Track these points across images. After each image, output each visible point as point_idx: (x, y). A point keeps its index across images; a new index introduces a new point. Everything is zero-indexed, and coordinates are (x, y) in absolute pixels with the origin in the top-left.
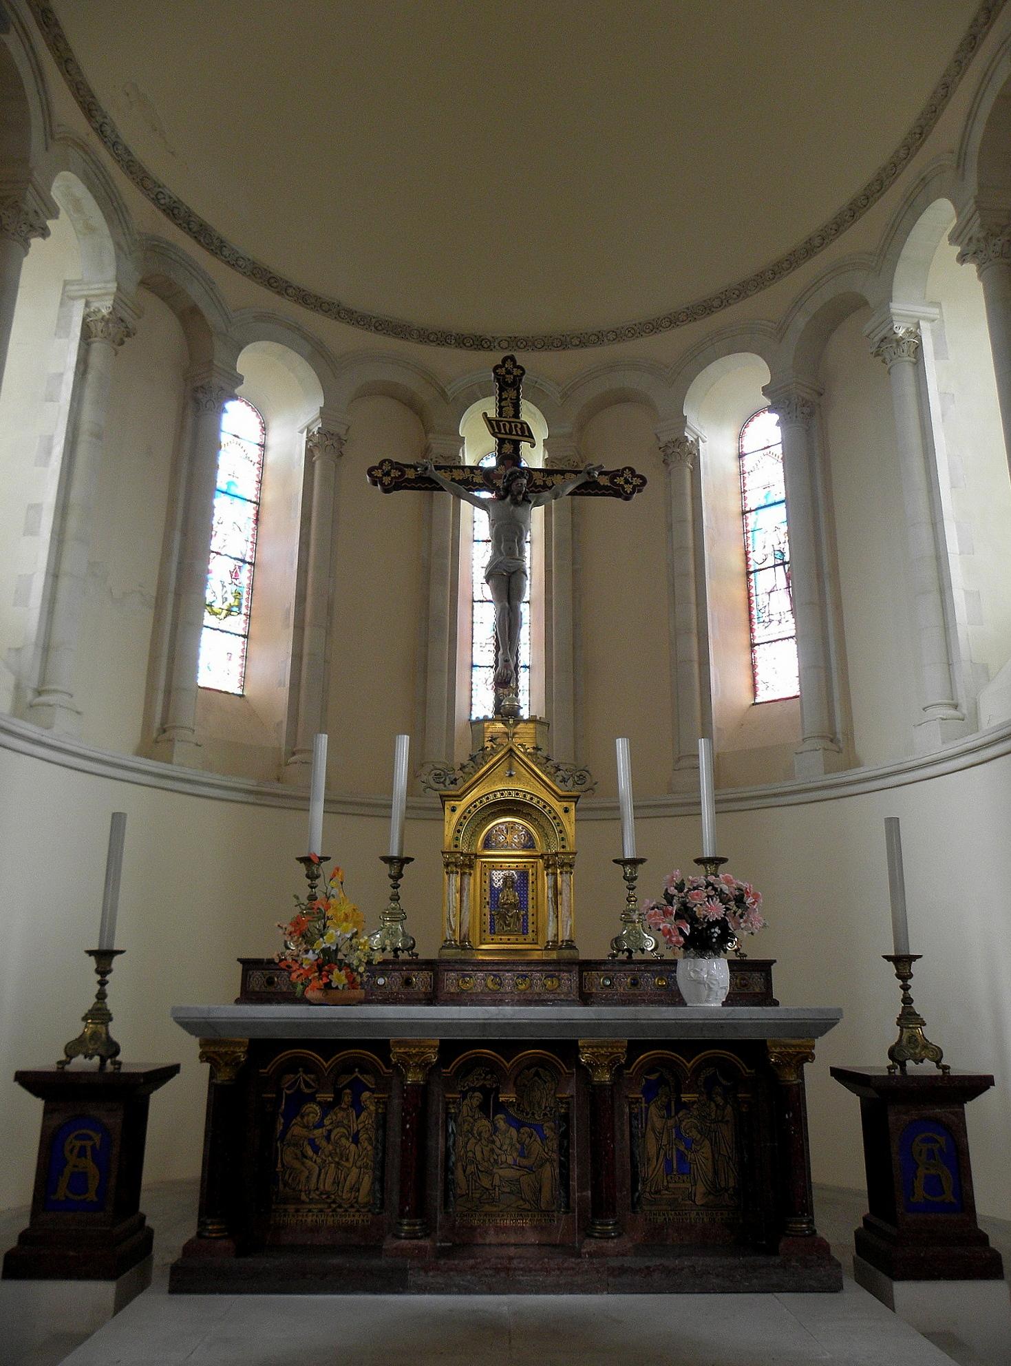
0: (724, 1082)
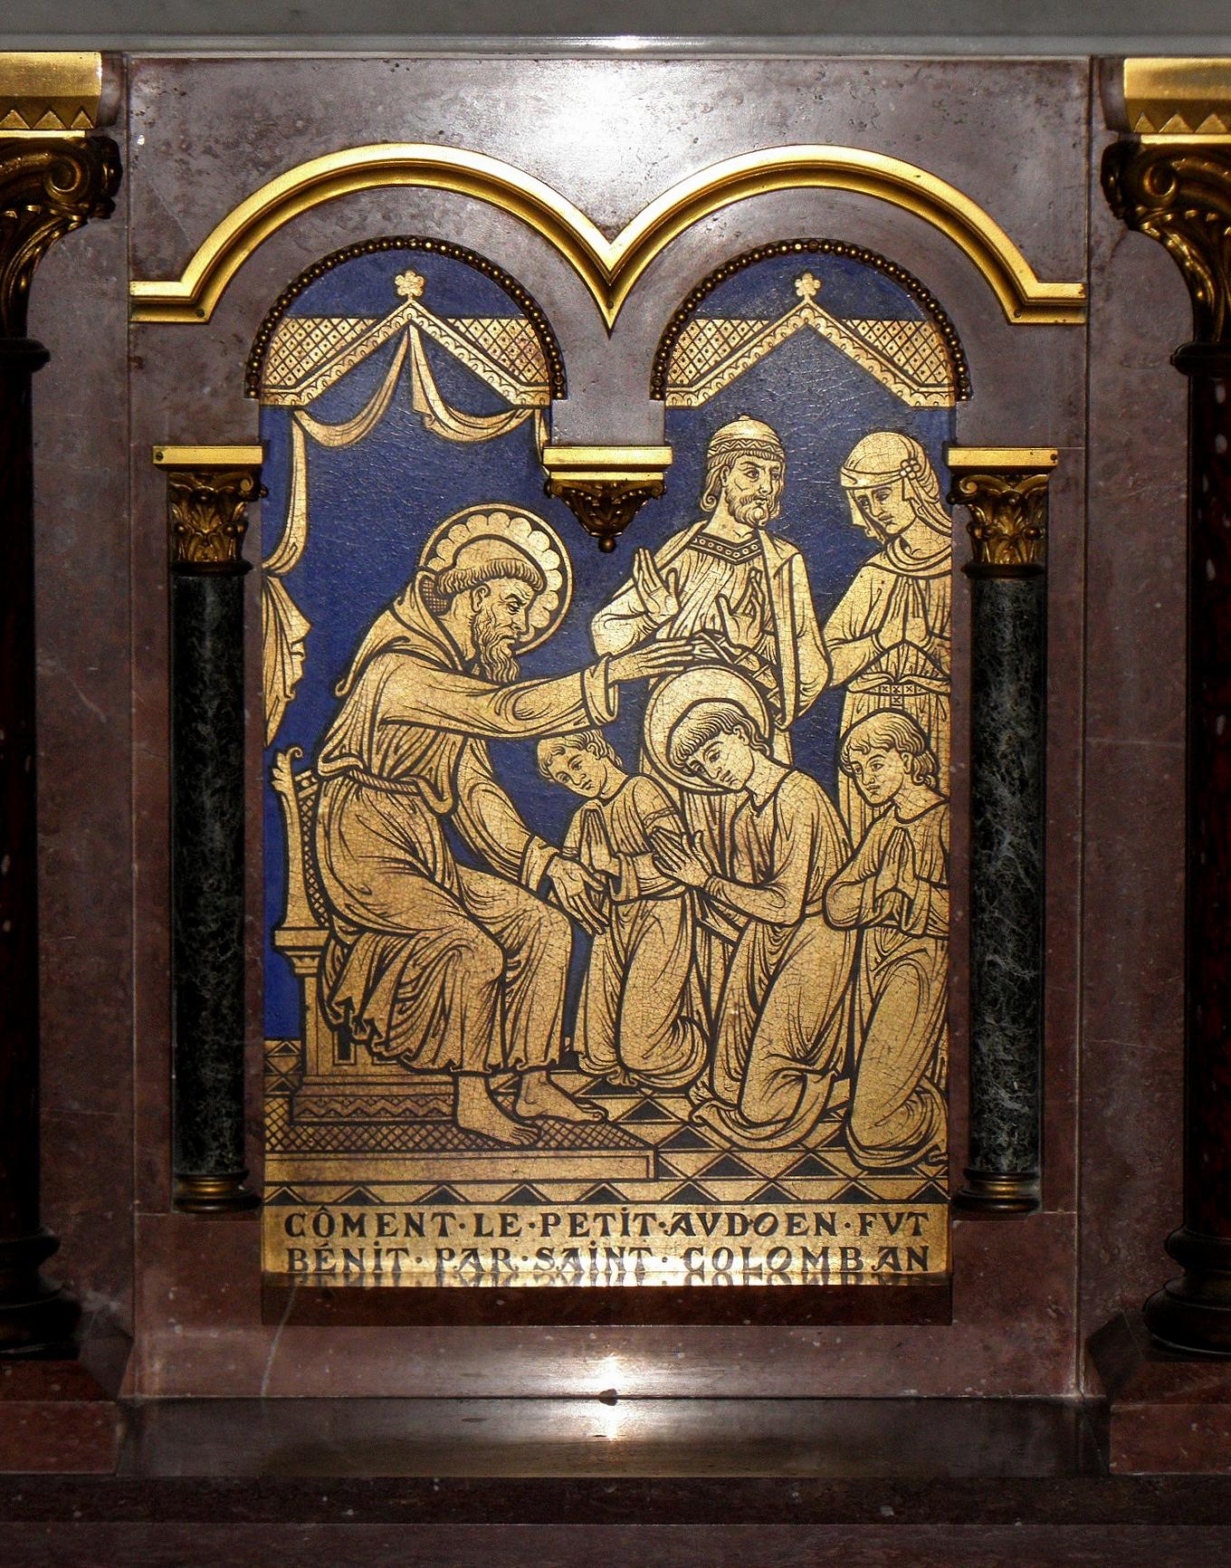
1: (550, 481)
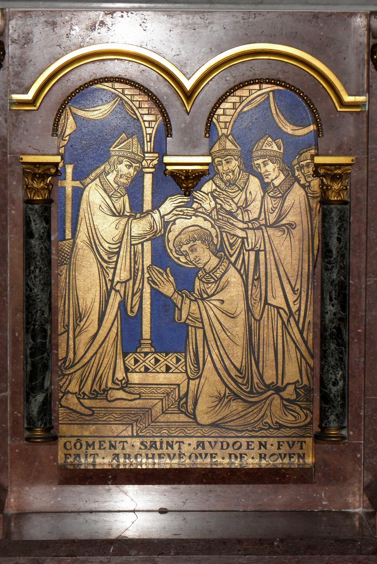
0: (289, 129)
1: (166, 170)
